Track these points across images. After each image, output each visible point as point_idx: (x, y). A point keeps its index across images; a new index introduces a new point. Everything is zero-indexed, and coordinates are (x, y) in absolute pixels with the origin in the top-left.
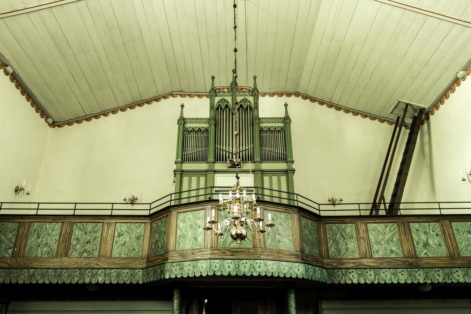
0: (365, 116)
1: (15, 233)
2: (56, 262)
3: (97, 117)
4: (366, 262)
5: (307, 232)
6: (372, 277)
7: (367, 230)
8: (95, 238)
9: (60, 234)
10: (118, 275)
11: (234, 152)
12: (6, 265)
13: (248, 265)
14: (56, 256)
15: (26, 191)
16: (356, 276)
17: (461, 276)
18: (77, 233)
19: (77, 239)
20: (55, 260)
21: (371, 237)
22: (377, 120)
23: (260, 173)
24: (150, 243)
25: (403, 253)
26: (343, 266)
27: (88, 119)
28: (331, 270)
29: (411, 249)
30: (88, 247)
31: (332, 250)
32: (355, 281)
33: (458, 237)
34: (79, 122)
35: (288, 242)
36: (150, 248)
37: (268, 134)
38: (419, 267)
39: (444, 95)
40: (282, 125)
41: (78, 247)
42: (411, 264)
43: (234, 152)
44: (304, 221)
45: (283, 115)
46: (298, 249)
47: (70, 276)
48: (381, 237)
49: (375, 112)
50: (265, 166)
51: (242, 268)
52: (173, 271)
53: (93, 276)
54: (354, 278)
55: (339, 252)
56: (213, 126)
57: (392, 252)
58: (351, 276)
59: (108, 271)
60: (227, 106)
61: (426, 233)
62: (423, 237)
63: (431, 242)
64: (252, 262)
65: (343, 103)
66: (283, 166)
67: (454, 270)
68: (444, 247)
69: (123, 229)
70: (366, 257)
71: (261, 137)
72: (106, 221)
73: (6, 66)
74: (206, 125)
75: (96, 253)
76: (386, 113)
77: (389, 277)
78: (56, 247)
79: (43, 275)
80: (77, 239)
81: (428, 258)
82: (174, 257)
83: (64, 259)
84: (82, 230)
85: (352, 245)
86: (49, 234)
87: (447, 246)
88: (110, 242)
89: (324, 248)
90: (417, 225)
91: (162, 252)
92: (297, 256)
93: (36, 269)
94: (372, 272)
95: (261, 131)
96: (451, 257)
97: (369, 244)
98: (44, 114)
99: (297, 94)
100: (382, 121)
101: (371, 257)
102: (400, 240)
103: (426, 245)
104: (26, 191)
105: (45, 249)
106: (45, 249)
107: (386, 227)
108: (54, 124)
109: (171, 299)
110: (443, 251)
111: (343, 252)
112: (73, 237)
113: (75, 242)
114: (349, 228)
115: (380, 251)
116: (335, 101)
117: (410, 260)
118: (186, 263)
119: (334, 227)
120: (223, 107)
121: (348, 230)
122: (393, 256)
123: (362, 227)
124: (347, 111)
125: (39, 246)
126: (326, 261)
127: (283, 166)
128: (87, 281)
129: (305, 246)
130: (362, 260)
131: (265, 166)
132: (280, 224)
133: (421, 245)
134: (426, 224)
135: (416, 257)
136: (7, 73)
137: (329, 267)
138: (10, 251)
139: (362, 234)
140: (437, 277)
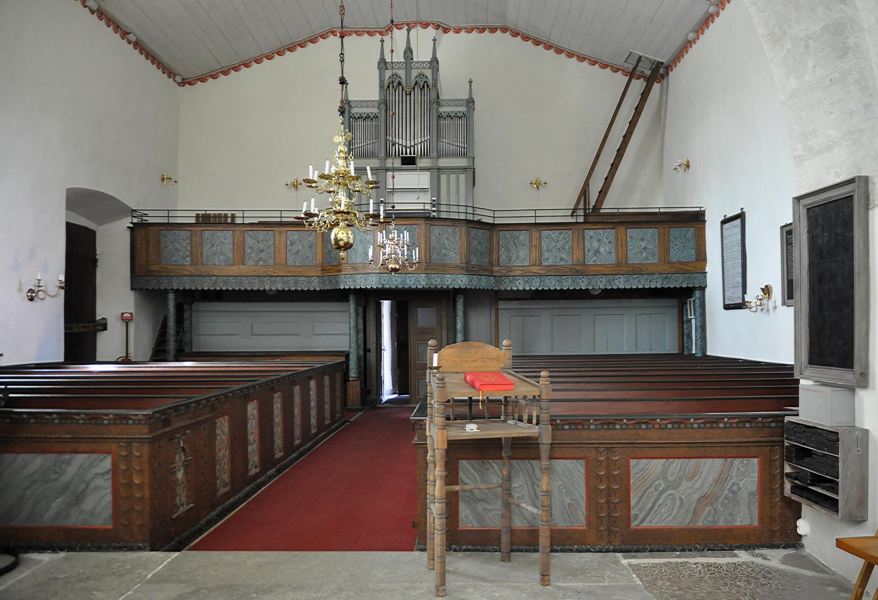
0: (594, 63)
1: (188, 241)
2: (235, 270)
3: (236, 69)
4: (534, 269)
5: (476, 242)
6: (537, 284)
7: (540, 237)
8: (268, 247)
9: (233, 243)
10: (296, 283)
11: (408, 145)
12: (188, 273)
13: (413, 279)
14: (234, 264)
15: (173, 180)
16: (522, 283)
17: (622, 282)
18: (250, 242)
19: (251, 248)
20: (233, 268)
21: (543, 244)
22: (609, 69)
23: (437, 171)
24: (323, 253)
25: (572, 260)
26: (512, 274)
27: (225, 73)
28: (499, 278)
29: (581, 256)
30: (262, 255)
31: (503, 258)
32: (521, 288)
33: (630, 244)
34: (214, 77)
35: (453, 255)
36: (323, 257)
37: (447, 122)
38: (583, 274)
39: (687, 45)
40: (463, 109)
41: (253, 255)
42: (577, 271)
43: (408, 145)
44: (474, 232)
45: (467, 97)
46: (464, 261)
47: (250, 283)
48: (553, 244)
49: (605, 59)
50: (443, 162)
51: (408, 281)
52: (346, 283)
53: (273, 283)
54: (520, 285)
55: (510, 259)
56: (383, 112)
57: (562, 259)
58: (517, 283)
59: (286, 279)
60: (399, 84)
61: (599, 240)
62: (595, 245)
63: (602, 250)
64: (416, 276)
65: (564, 45)
66: (462, 162)
67: (617, 277)
68: (613, 255)
69: (294, 237)
70: (535, 265)
71: (438, 126)
72: (276, 229)
73: (129, 33)
74: (375, 110)
75: (271, 262)
76: (620, 62)
77: (553, 283)
78: (231, 256)
79: (225, 283)
80: (251, 248)
81: (596, 265)
82: (347, 270)
83: (242, 267)
84: (253, 238)
85: (523, 253)
86: (222, 243)
87: (617, 254)
88: (283, 251)
89: (495, 256)
90: (592, 232)
91: (335, 264)
92: (462, 268)
93: (217, 276)
94: (538, 280)
95: (439, 117)
96: (618, 264)
97: (540, 252)
98: (170, 73)
99: (505, 30)
100: (615, 70)
101: (540, 264)
102: (572, 248)
103: (597, 252)
104: (173, 180)
105: (222, 257)
106: (222, 257)
107: (560, 234)
108: (183, 83)
109: (348, 300)
110: (612, 259)
111: (513, 259)
112: (247, 245)
113: (249, 251)
114: (523, 236)
115: (549, 259)
116: (554, 41)
117: (577, 268)
118: (358, 276)
119: (508, 234)
120: (395, 84)
121: (521, 238)
122: (562, 263)
123: (535, 234)
124: (570, 55)
125: (214, 254)
126: (496, 269)
127: (462, 162)
128: (267, 288)
129: (472, 257)
130: (531, 268)
131: (443, 162)
132: (447, 238)
133: (592, 252)
134: (601, 231)
135: (584, 264)
136: (129, 42)
137: (498, 274)
138: (188, 259)
139: (535, 242)
140: (599, 284)
